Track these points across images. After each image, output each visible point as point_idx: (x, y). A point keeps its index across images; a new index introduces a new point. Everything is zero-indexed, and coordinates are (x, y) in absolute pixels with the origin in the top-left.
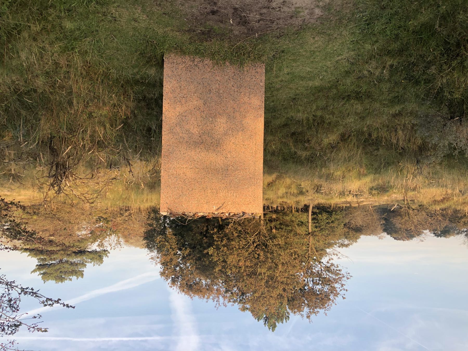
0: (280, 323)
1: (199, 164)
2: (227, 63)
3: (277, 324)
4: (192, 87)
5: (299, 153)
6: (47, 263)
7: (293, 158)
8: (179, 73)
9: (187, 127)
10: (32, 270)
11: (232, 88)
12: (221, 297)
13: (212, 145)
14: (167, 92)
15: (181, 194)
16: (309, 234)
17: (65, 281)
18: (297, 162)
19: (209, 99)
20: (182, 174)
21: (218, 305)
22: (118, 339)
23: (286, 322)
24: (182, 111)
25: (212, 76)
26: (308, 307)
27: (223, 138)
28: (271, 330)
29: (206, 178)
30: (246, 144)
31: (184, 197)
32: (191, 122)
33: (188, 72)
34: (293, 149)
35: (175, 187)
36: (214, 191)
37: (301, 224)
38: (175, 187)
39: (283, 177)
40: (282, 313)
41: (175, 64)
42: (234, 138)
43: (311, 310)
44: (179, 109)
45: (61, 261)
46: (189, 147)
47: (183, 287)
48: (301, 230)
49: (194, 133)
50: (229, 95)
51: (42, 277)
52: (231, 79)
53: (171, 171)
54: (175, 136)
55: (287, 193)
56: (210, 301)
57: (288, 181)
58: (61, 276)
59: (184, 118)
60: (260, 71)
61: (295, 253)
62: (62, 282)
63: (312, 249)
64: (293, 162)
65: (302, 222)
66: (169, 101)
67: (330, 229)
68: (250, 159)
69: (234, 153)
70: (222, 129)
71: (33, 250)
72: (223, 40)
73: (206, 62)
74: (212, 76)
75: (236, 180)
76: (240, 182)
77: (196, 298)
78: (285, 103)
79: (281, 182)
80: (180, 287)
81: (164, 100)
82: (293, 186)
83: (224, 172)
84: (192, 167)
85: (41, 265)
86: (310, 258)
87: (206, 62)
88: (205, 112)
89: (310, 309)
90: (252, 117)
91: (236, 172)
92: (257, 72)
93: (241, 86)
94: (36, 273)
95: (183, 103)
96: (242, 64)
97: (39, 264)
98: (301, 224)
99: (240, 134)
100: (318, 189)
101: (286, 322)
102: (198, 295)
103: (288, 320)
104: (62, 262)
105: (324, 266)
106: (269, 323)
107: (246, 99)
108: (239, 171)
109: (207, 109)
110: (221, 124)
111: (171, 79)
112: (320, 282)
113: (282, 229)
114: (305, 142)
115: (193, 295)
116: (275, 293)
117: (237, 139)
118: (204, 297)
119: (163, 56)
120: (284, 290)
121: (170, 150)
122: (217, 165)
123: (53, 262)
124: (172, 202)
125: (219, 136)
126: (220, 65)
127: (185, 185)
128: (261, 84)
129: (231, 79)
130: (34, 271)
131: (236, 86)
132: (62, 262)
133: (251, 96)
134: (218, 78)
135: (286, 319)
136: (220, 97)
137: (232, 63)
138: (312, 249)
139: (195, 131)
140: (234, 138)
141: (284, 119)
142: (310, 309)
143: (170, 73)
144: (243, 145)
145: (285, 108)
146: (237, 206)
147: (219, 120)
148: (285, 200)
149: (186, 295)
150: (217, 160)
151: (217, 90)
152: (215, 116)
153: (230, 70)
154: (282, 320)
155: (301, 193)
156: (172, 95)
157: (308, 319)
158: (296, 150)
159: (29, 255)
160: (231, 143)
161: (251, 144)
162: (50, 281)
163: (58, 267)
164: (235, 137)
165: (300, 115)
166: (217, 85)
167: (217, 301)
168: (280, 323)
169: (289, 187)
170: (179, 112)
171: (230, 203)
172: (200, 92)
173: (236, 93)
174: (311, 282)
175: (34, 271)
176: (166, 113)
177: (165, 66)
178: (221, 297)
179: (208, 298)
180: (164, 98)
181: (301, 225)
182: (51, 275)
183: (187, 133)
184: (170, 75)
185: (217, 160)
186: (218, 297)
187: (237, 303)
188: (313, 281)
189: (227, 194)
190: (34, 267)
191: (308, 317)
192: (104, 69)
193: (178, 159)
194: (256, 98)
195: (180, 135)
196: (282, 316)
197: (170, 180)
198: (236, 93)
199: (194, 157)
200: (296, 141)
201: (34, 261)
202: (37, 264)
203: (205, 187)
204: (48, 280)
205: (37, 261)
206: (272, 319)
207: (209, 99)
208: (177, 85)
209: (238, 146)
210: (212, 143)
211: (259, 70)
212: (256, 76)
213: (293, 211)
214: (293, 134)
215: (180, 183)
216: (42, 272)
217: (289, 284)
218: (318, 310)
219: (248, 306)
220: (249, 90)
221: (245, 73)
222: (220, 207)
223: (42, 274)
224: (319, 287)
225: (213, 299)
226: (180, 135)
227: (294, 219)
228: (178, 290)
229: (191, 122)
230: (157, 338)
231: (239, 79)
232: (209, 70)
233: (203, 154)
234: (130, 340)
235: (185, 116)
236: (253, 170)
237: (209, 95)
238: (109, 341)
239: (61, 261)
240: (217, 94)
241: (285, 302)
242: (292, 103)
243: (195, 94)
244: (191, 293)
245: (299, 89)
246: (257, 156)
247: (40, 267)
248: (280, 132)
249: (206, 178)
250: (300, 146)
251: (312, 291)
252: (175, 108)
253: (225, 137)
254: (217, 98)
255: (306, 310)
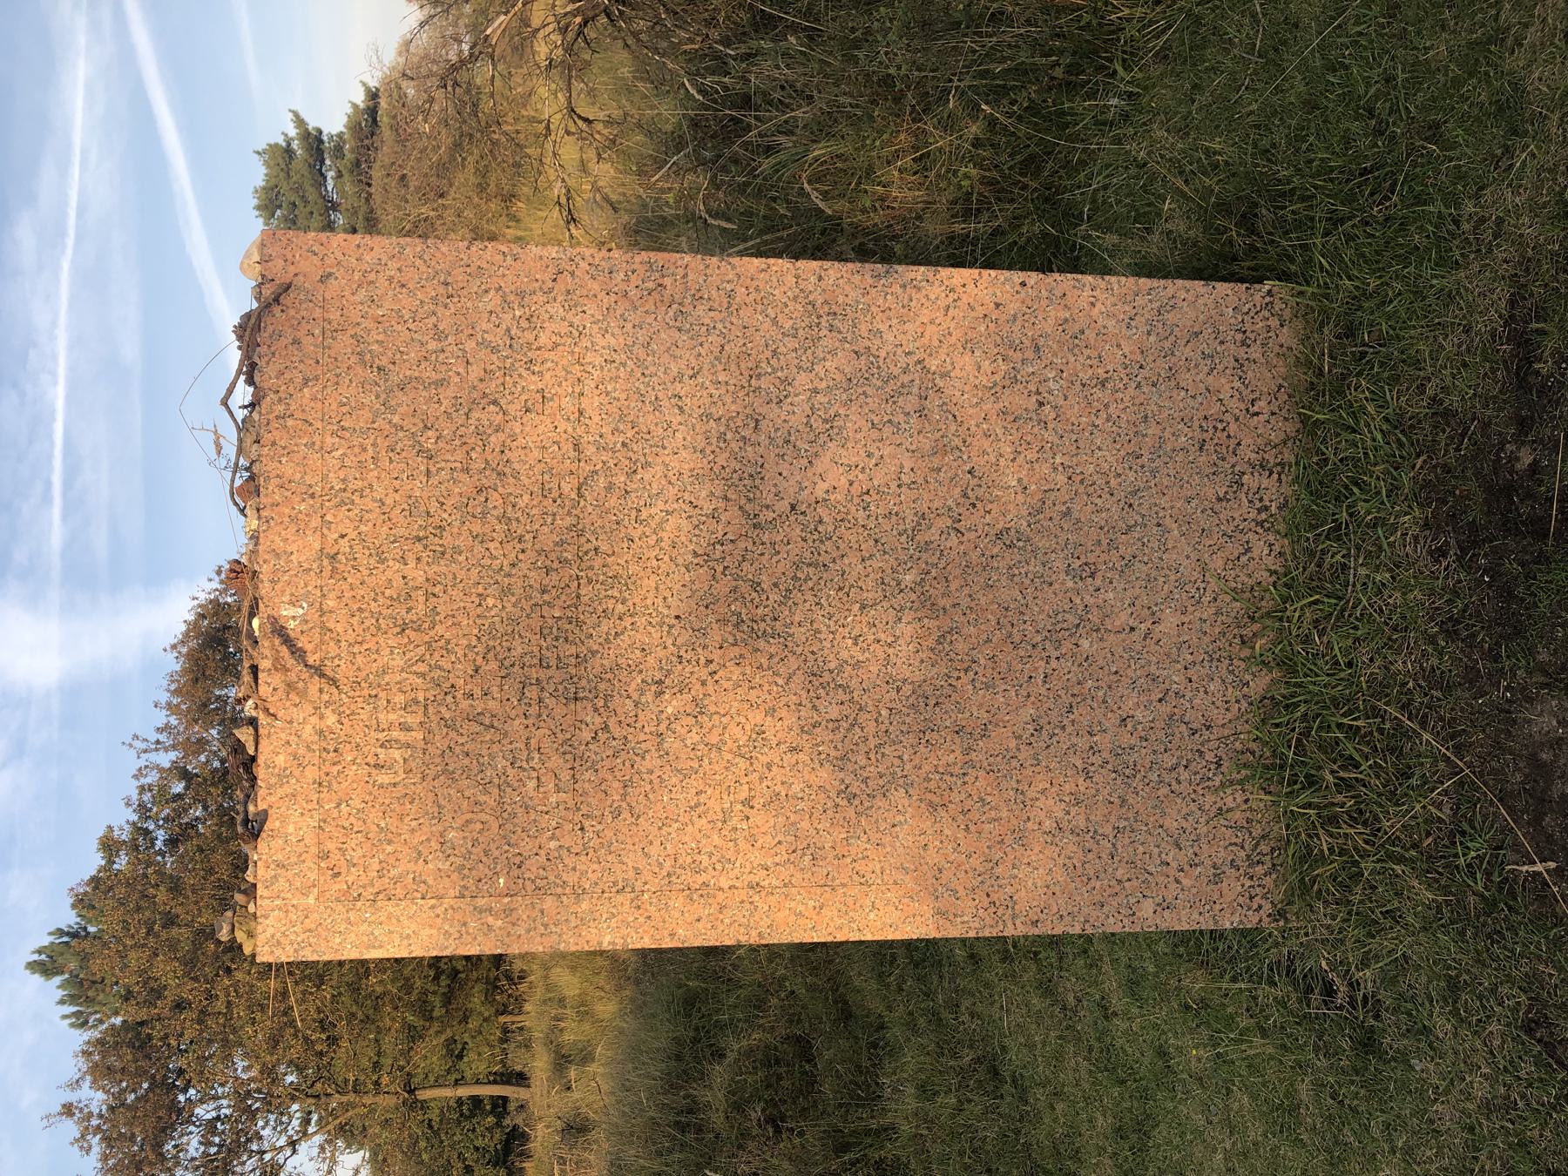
0: (61, 993)
1: (613, 501)
2: (1259, 684)
3: (58, 980)
4: (1109, 457)
5: (719, 1074)
6: (328, 162)
7: (695, 1041)
8: (1186, 378)
9: (854, 421)
10: (303, 115)
11: (1114, 719)
12: (173, 755)
13: (744, 588)
14: (1070, 300)
15: (395, 379)
16: (411, 1092)
17: (261, 220)
18: (679, 1058)
19: (1035, 567)
20: (534, 383)
21: (144, 746)
22: (60, 404)
23: (65, 1017)
24: (952, 389)
25: (1181, 585)
26: (112, 1109)
27: (793, 663)
28: (36, 957)
29: (511, 551)
30: (758, 818)
31: (369, 399)
32: (886, 451)
33: (1198, 434)
34: (734, 1046)
35: (439, 336)
36: (421, 608)
37: (455, 1052)
38: (439, 336)
39: (619, 988)
40: (101, 996)
41: (1242, 355)
42: (793, 738)
43: (95, 1122)
44: (967, 372)
45: (335, 207)
46: (722, 437)
47: (216, 614)
48: (429, 1055)
49: (819, 466)
50: (1067, 700)
51: (276, 145)
52: (1165, 709)
53: (556, 309)
54: (791, 343)
55: (562, 1001)
56: (161, 717)
57: (606, 1008)
58: (280, 207)
59: (911, 403)
60: (1229, 896)
61: (333, 1041)
62: (258, 208)
63: (346, 1107)
64: (678, 1041)
65: (460, 1057)
66: (1013, 307)
67: (441, 1161)
68: (654, 850)
69: (693, 738)
70: (849, 651)
71: (375, 121)
72: (1451, 635)
73: (1259, 548)
74: (1181, 585)
75: (501, 763)
76: (485, 786)
77: (173, 664)
78: (965, 1018)
79: (601, 980)
80: (215, 602)
81: (1017, 276)
82: (587, 1026)
83: (558, 676)
84: (590, 451)
85: (322, 142)
86: (312, 1101)
87: (1259, 548)
88: (954, 540)
89: (101, 1116)
90: (933, 857)
91: (555, 761)
92: (1217, 879)
93: (1127, 772)
94: (292, 125)
95: (1006, 399)
96: (854, 799)
97: (325, 138)
98: (455, 1052)
99: (824, 775)
100: (575, 1129)
101: (65, 1017)
102: (184, 671)
103: (72, 1025)
104: (327, 209)
105: (281, 1161)
106: (62, 948)
107: (1047, 810)
108: (565, 776)
109: (974, 556)
110: (879, 646)
111: (1149, 322)
112: (213, 1150)
113: (436, 978)
114: (771, 1103)
115: (184, 650)
116: (166, 970)
117: (790, 759)
118: (176, 692)
119: (1284, 277)
120: (179, 1006)
121: (701, 309)
122: (605, 626)
123: (330, 184)
124: (334, 315)
125: (800, 633)
126: (1247, 632)
127: (457, 406)
128: (1147, 907)
129: (1165, 709)
130: (300, 122)
131: (1127, 740)
132: (327, 209)
133: (1070, 845)
134: (1170, 620)
135: (77, 1014)
136: (1053, 635)
137: (1270, 708)
138: (346, 1107)
139: (832, 475)
140: (793, 738)
141: (876, 1006)
142: (101, 1116)
143: (1184, 317)
144: (747, 803)
145: (936, 1019)
146: (311, 773)
147: (906, 630)
148: (539, 993)
149: (183, 628)
150: (641, 621)
151: (1095, 617)
152: (928, 606)
153: (1223, 699)
154: (72, 999)
155: (562, 1061)
156: (1049, 326)
157: (59, 1108)
158: (731, 1057)
159: (355, 106)
160: (757, 717)
161: (756, 857)
162: (263, 170)
163: (312, 195)
164: (804, 742)
165: (910, 1101)
166: (1123, 619)
167: (158, 742)
168: (61, 993)
169: (584, 1011)
170: (944, 375)
171: (331, 720)
172: (1076, 507)
173: (1083, 743)
174: (214, 1114)
175: (300, 122)
176: (935, 291)
177: (1223, 288)
178: (173, 755)
179: (169, 706)
180: (1033, 277)
181: (450, 1052)
182: (282, 175)
183: (817, 424)
184: (1170, 317)
185: (641, 621)
186: (174, 747)
187: (134, 817)
188: (218, 1118)
189: (399, 699)
190: (312, 124)
191: (68, 1110)
192: (1131, 31)
193: (639, 362)
194: (1060, 876)
195: (802, 379)
196: (90, 1001)
197: (492, 301)
198: (1083, 743)
199: (659, 469)
200: (770, 1059)
201: (333, 121)
202: (325, 132)
203: (447, 540)
204: (266, 163)
205: (334, 132)
206: (71, 962)
207: (1035, 567)
208: (1113, 359)
209: (743, 764)
210: (756, 586)
211: (1233, 887)
212: (1198, 872)
213: (502, 1019)
214: (804, 1048)
215: (475, 372)
216: (295, 145)
217: (200, 1022)
218: (97, 1150)
219: (122, 863)
220: (1108, 830)
221: (1210, 799)
222: (298, 653)
223: (289, 145)
224: (194, 1146)
225: (166, 728)
226: (802, 379)
227: (473, 1024)
228: (203, 597)
229: (886, 451)
230: (56, 535)
231: (1170, 761)
232: (1218, 563)
233: (678, 526)
234: (52, 444)
235: (921, 413)
236: (571, 878)
237: (1060, 565)
238: (54, 374)
239: (335, 207)
240: (1072, 619)
241: (136, 1013)
242: (968, 1057)
243: (1061, 479)
244: (193, 644)
245: (1060, 1107)
246: (677, 902)
247: (313, 141)
248: (811, 988)
249: (511, 551)
250: (754, 1079)
251: (178, 1116)
252: (968, 345)
253: (799, 678)
254: (1044, 622)
255: (95, 1099)
